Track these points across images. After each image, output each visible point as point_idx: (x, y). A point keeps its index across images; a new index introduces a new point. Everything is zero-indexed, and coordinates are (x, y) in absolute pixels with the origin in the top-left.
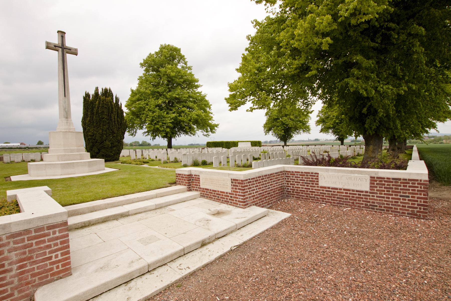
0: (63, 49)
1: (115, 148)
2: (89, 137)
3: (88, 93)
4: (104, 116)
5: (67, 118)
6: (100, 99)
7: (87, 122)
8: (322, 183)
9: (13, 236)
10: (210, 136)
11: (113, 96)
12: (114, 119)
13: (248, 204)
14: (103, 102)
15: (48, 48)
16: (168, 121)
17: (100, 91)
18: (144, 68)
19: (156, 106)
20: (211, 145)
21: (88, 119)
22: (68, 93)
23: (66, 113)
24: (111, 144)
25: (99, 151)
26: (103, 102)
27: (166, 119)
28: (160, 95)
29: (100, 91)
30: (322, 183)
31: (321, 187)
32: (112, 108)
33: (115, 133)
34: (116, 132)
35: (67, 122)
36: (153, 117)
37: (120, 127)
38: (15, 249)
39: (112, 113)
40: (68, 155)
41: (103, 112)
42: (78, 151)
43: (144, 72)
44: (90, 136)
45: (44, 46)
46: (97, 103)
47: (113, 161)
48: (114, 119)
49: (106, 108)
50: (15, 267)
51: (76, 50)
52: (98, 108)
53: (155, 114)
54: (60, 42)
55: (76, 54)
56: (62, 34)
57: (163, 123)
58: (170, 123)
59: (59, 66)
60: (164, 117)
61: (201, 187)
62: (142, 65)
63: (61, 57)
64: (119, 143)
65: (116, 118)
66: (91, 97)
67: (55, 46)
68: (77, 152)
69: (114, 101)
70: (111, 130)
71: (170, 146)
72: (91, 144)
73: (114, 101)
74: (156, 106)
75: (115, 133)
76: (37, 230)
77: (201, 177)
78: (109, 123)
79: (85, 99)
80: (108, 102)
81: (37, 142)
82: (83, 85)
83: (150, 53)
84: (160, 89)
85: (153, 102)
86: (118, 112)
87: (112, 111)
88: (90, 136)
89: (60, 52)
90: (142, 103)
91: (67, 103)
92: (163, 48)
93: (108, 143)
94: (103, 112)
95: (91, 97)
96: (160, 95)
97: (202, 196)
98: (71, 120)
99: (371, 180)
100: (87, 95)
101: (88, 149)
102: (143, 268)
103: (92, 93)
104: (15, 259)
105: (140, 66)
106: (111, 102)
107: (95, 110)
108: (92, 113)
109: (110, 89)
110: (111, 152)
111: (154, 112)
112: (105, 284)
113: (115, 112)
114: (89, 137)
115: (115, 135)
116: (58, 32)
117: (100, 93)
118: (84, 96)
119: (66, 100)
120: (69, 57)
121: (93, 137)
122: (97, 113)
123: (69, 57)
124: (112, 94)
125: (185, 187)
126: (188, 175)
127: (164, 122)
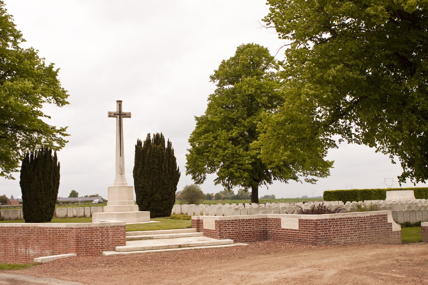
0: (120, 115)
1: (165, 202)
2: (140, 189)
3: (140, 141)
4: (154, 166)
5: (121, 174)
6: (151, 147)
7: (137, 173)
8: (283, 226)
9: (111, 227)
10: (317, 182)
11: (164, 142)
12: (165, 168)
13: (223, 237)
14: (153, 150)
15: (110, 116)
16: (247, 162)
17: (152, 137)
18: (217, 82)
19: (230, 140)
20: (329, 196)
21: (139, 169)
22: (123, 152)
23: (121, 171)
24: (162, 197)
25: (149, 205)
26: (153, 150)
27: (244, 158)
28: (234, 122)
29: (152, 137)
30: (283, 226)
31: (283, 229)
32: (163, 157)
33: (165, 184)
34: (167, 183)
35: (122, 178)
36: (224, 156)
37: (171, 177)
38: (112, 231)
39: (163, 161)
40: (122, 207)
41: (154, 161)
42: (129, 203)
43: (216, 88)
44: (141, 188)
45: (107, 115)
46: (148, 152)
47: (164, 216)
48: (165, 168)
49: (157, 157)
50: (111, 237)
51: (130, 114)
52: (149, 157)
53: (227, 151)
54: (118, 110)
55: (130, 117)
56: (120, 103)
57: (238, 165)
58: (249, 163)
59: (117, 130)
60: (240, 156)
61: (204, 228)
62: (213, 78)
63: (118, 123)
64: (170, 195)
65: (167, 166)
66: (143, 144)
67: (115, 114)
68: (129, 204)
69: (166, 146)
70: (162, 181)
71: (254, 198)
72: (141, 197)
73: (166, 146)
74: (230, 140)
75: (165, 184)
76: (117, 227)
77: (204, 221)
78: (159, 173)
79: (137, 147)
80: (158, 151)
81: (70, 192)
82: (137, 132)
83: (224, 60)
84: (234, 115)
85: (223, 134)
86: (169, 160)
87: (163, 159)
88: (141, 188)
89: (118, 118)
90: (210, 136)
91: (122, 161)
92: (241, 51)
93: (158, 196)
94: (154, 161)
95: (143, 144)
96: (234, 122)
97: (205, 235)
98: (125, 176)
99: (299, 222)
100: (139, 143)
101: (138, 202)
102: (150, 247)
103: (143, 139)
104: (111, 235)
105: (210, 79)
106: (161, 150)
107: (146, 159)
108: (144, 164)
109: (161, 134)
110: (162, 206)
111: (225, 149)
112: (136, 248)
113: (166, 160)
114: (140, 189)
115: (166, 186)
116: (117, 101)
117: (151, 139)
118: (136, 144)
119: (122, 159)
120: (124, 120)
121: (144, 189)
122: (148, 163)
123: (124, 120)
124: (164, 140)
125: (196, 229)
126: (197, 220)
127: (241, 162)
